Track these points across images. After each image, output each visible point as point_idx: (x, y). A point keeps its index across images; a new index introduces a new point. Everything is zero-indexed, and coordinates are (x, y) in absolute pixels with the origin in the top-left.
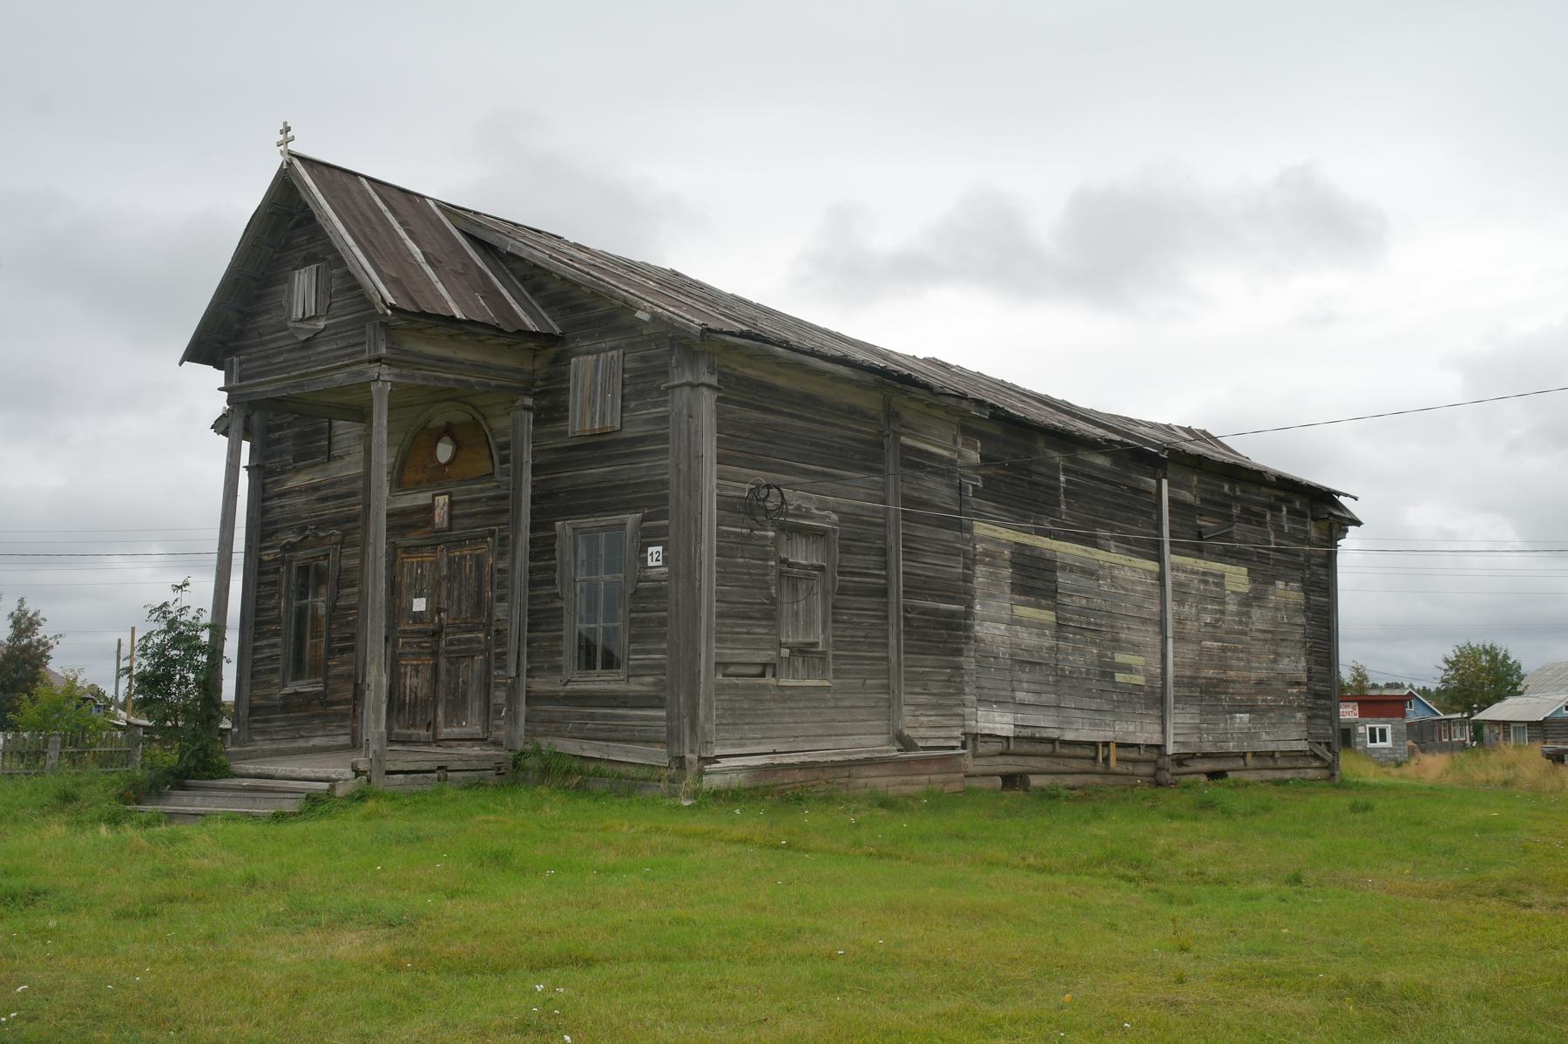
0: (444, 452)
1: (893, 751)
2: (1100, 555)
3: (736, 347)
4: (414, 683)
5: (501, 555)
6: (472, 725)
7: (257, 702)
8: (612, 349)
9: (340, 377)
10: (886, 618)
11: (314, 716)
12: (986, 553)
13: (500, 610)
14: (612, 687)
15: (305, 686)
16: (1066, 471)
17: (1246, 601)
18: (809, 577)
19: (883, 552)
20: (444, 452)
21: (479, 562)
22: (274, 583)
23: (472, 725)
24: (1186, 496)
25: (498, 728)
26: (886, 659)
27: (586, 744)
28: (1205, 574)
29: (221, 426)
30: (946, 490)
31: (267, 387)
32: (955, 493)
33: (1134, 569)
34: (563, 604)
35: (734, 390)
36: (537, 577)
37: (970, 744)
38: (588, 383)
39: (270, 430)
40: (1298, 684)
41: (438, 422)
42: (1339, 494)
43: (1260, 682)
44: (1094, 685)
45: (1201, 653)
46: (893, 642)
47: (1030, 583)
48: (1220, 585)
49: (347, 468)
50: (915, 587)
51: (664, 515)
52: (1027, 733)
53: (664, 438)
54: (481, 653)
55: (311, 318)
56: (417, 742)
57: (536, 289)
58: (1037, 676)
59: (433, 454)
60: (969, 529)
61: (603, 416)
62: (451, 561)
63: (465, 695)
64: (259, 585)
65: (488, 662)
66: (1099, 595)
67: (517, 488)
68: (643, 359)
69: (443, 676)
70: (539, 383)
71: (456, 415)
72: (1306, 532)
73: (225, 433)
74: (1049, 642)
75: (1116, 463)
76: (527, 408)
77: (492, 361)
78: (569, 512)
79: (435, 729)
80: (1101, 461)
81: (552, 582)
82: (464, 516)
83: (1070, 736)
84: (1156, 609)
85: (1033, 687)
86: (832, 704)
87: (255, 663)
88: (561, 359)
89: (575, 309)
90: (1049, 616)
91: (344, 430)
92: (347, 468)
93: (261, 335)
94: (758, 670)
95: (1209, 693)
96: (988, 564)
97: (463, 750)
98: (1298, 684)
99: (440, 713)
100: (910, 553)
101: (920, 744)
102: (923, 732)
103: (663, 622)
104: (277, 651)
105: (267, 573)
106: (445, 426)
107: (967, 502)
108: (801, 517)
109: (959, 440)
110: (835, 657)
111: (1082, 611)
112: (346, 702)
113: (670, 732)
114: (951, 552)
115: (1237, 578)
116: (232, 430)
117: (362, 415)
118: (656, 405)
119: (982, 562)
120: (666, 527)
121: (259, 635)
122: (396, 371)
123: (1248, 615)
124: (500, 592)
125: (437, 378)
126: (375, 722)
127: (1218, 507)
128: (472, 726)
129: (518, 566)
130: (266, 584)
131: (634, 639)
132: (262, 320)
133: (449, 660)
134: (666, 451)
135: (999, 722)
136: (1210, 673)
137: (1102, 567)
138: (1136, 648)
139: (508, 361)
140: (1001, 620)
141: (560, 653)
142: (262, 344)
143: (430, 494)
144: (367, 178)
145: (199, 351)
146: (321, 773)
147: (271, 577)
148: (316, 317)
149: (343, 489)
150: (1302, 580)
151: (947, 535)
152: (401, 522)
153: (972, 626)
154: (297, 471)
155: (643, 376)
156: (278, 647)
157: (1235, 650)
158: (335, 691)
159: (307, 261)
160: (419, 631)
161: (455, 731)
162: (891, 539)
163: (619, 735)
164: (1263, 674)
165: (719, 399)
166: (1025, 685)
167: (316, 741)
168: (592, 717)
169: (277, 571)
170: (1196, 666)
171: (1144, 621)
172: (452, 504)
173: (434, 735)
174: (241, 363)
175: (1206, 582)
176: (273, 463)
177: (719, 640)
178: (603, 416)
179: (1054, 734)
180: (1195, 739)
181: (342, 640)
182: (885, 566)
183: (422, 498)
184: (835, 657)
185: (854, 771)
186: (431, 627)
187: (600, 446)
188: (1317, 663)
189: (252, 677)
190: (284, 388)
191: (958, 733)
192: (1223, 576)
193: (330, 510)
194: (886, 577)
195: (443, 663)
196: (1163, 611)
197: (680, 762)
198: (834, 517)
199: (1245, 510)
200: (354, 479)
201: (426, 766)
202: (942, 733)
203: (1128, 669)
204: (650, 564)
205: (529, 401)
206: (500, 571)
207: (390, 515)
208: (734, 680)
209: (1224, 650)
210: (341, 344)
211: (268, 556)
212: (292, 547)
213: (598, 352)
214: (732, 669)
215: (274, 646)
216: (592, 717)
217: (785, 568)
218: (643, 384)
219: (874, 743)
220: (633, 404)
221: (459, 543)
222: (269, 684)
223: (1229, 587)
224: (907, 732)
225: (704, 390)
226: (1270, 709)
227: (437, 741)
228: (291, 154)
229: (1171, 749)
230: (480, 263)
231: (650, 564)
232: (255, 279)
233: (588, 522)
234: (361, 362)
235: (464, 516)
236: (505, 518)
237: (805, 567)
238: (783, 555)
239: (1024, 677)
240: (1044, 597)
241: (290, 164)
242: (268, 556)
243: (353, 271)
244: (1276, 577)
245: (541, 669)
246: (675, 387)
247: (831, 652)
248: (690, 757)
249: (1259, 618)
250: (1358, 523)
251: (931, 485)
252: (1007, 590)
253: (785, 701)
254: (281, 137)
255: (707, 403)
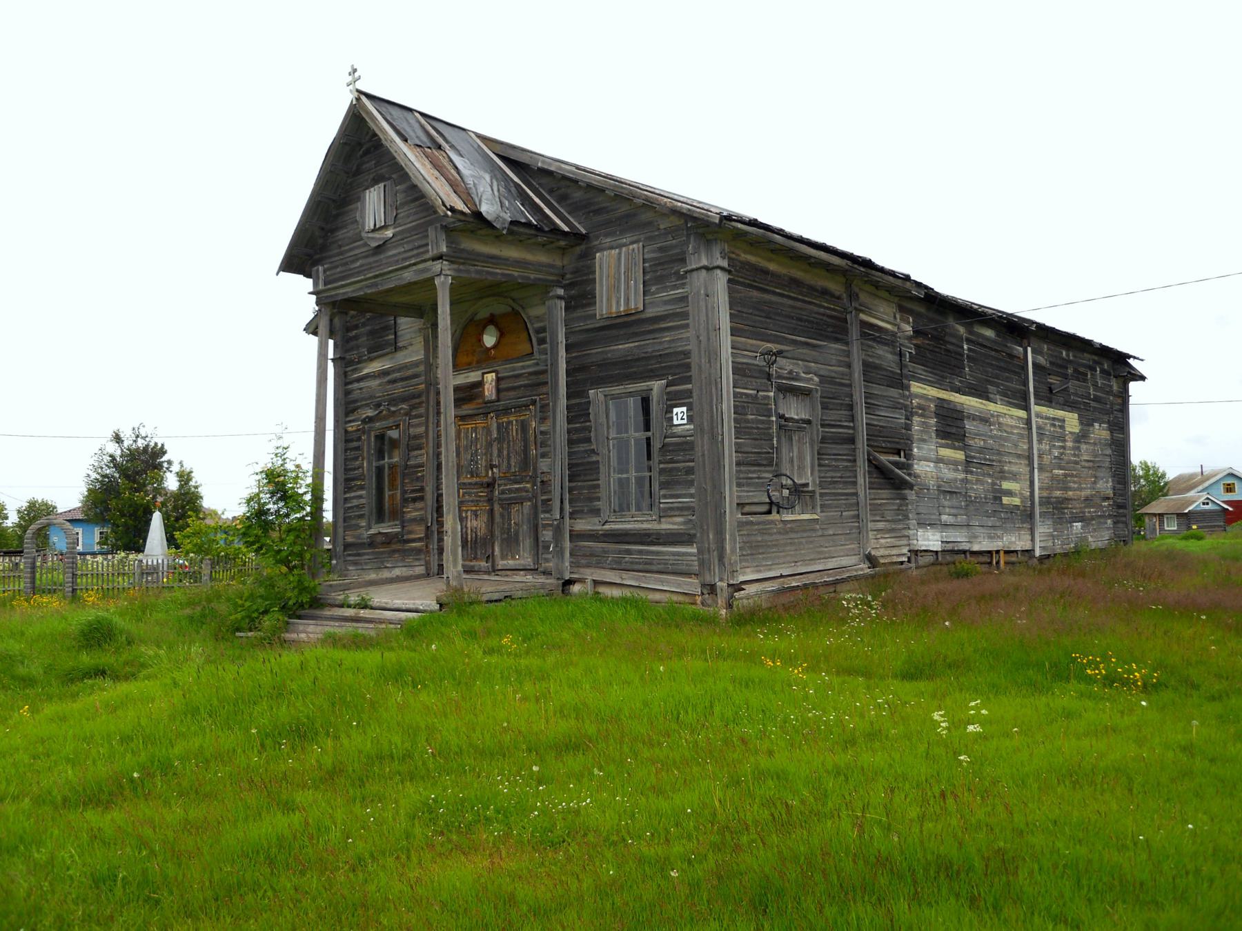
0: (489, 340)
1: (864, 569)
2: (991, 407)
3: (746, 233)
4: (478, 524)
5: (543, 420)
6: (524, 558)
7: (350, 540)
8: (632, 243)
9: (408, 276)
10: (855, 461)
11: (394, 551)
12: (920, 407)
13: (543, 465)
14: (645, 526)
15: (387, 528)
16: (969, 341)
17: (1081, 438)
18: (800, 429)
19: (851, 407)
20: (489, 340)
21: (524, 427)
22: (358, 448)
23: (524, 558)
24: (1041, 360)
25: (547, 560)
26: (856, 494)
27: (625, 575)
28: (1054, 419)
29: (312, 328)
30: (890, 356)
31: (348, 290)
32: (897, 358)
33: (1011, 417)
34: (599, 458)
35: (741, 276)
36: (575, 437)
37: (913, 559)
38: (613, 271)
39: (348, 330)
40: (1108, 498)
41: (483, 314)
42: (1130, 357)
43: (1087, 499)
44: (990, 508)
45: (1053, 478)
46: (860, 480)
47: (949, 429)
48: (1062, 427)
49: (413, 354)
50: (875, 434)
51: (688, 380)
52: (949, 547)
53: (685, 315)
54: (530, 500)
55: (381, 228)
56: (478, 572)
57: (562, 199)
58: (955, 502)
59: (480, 340)
60: (908, 388)
61: (627, 300)
62: (499, 427)
63: (517, 534)
64: (346, 450)
65: (535, 507)
66: (991, 437)
67: (555, 364)
68: (661, 249)
69: (497, 518)
70: (568, 276)
71: (499, 308)
72: (1111, 387)
73: (315, 333)
74: (961, 476)
75: (998, 335)
76: (560, 297)
77: (529, 257)
78: (599, 382)
79: (493, 562)
80: (989, 333)
81: (588, 440)
82: (508, 389)
83: (976, 548)
84: (1025, 447)
85: (953, 511)
86: (820, 533)
87: (346, 510)
88: (588, 255)
89: (598, 212)
90: (960, 455)
91: (408, 326)
92: (413, 354)
93: (340, 246)
94: (765, 508)
95: (1058, 509)
96: (922, 416)
97: (518, 578)
98: (1108, 498)
99: (497, 549)
100: (870, 407)
101: (882, 561)
102: (882, 552)
103: (690, 471)
104: (363, 501)
105: (352, 441)
106: (493, 310)
107: (906, 366)
108: (793, 379)
109: (898, 316)
110: (822, 495)
111: (982, 450)
112: (420, 540)
113: (702, 563)
114: (896, 407)
115: (1072, 421)
116: (320, 331)
117: (426, 312)
118: (675, 287)
119: (917, 413)
120: (690, 391)
121: (348, 489)
122: (455, 266)
123: (1078, 448)
124: (541, 450)
125: (488, 273)
126: (454, 563)
127: (1059, 367)
128: (525, 559)
129: (558, 428)
130: (351, 449)
131: (663, 485)
132: (341, 234)
133: (502, 506)
134: (687, 326)
135: (930, 540)
136: (1058, 493)
137: (992, 416)
138: (1014, 477)
139: (542, 258)
140: (931, 462)
141: (598, 499)
142: (341, 253)
143: (480, 373)
144: (422, 114)
145: (295, 262)
146: (410, 604)
147: (355, 444)
148: (385, 227)
149: (410, 373)
150: (1109, 422)
151: (894, 392)
152: (467, 394)
153: (912, 465)
154: (371, 360)
155: (660, 264)
156: (363, 497)
157: (1072, 476)
158: (410, 532)
159: (376, 181)
160: (476, 484)
161: (511, 563)
162: (856, 397)
163: (654, 568)
164: (1088, 492)
165: (729, 281)
166: (947, 510)
167: (397, 572)
168: (629, 552)
169: (359, 439)
170: (1049, 488)
171: (1019, 456)
172: (498, 380)
173: (493, 566)
174: (325, 271)
175: (1054, 425)
176: (353, 355)
177: (739, 485)
178: (627, 300)
179: (966, 547)
180: (1050, 544)
181: (413, 491)
182: (852, 418)
183: (474, 376)
184: (822, 495)
185: (839, 587)
186: (486, 480)
187: (627, 325)
188: (1119, 483)
189: (345, 521)
190: (361, 289)
191: (905, 550)
192: (1064, 421)
193: (399, 389)
194: (853, 428)
195: (497, 507)
196: (1031, 448)
197: (712, 589)
198: (816, 379)
199: (1076, 370)
200: (416, 364)
201: (495, 596)
202: (895, 552)
203: (1009, 493)
204: (675, 422)
205: (561, 292)
206: (542, 433)
207: (457, 389)
208: (751, 518)
209: (1066, 475)
210: (407, 247)
211: (351, 427)
212: (370, 420)
213: (620, 246)
214: (747, 509)
215: (360, 497)
216: (629, 552)
217: (783, 422)
218: (664, 269)
219: (847, 561)
220: (653, 289)
221: (506, 411)
222: (358, 527)
223: (1068, 429)
224: (873, 553)
225: (719, 272)
226: (1092, 519)
227: (494, 570)
228: (358, 91)
229: (1037, 553)
230: (516, 179)
231: (675, 422)
232: (334, 201)
233: (616, 390)
234: (425, 261)
235: (508, 389)
236: (544, 389)
237: (797, 421)
238: (781, 412)
239: (946, 503)
240: (957, 440)
241: (358, 99)
242: (351, 427)
243: (415, 181)
244: (1094, 420)
245: (582, 512)
246: (692, 270)
247: (818, 491)
248: (721, 585)
249: (1086, 451)
250: (1143, 378)
251: (880, 352)
252: (934, 435)
253: (787, 533)
254: (350, 78)
255: (721, 279)
